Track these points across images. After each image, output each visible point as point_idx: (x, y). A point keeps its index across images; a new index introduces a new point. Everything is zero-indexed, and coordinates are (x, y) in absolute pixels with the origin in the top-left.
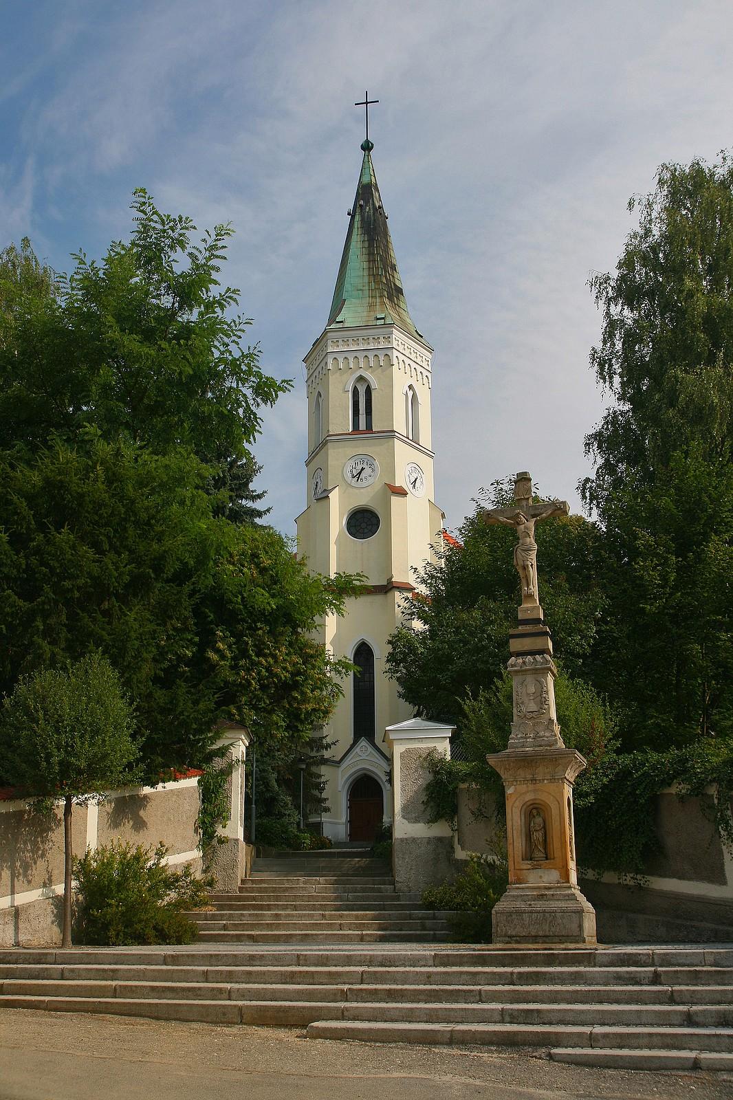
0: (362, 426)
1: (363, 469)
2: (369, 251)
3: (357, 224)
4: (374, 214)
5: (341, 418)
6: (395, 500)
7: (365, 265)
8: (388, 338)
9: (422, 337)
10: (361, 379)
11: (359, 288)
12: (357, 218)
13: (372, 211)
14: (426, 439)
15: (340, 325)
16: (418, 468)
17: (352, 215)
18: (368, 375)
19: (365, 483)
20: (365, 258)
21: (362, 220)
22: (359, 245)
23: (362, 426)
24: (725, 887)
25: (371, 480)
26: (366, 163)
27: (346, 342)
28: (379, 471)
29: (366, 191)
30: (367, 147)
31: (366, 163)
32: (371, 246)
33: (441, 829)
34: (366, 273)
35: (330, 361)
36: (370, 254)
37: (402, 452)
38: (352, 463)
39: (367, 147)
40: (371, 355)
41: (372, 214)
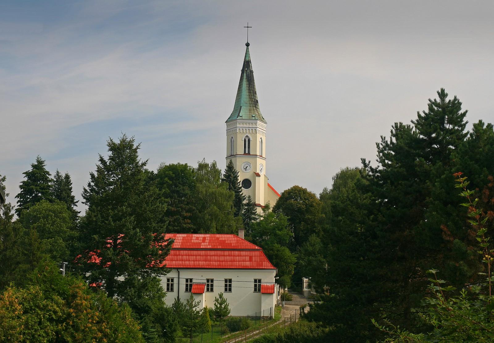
0: (247, 152)
1: (247, 167)
2: (249, 88)
3: (245, 77)
4: (250, 73)
5: (240, 150)
6: (257, 178)
7: (248, 94)
8: (256, 124)
9: (264, 119)
10: (247, 136)
11: (246, 102)
12: (245, 74)
13: (250, 72)
14: (264, 156)
15: (241, 118)
16: (262, 165)
17: (243, 71)
18: (249, 135)
19: (248, 171)
20: (248, 91)
21: (247, 75)
22: (246, 86)
23: (247, 152)
24: (462, 104)
25: (249, 171)
26: (247, 49)
27: (243, 124)
28: (252, 167)
29: (247, 64)
30: (248, 45)
31: (247, 49)
32: (249, 87)
33: (309, 290)
34: (248, 97)
35: (238, 130)
36: (249, 90)
37: (259, 161)
38: (244, 164)
39: (248, 45)
40: (250, 129)
41: (250, 73)
